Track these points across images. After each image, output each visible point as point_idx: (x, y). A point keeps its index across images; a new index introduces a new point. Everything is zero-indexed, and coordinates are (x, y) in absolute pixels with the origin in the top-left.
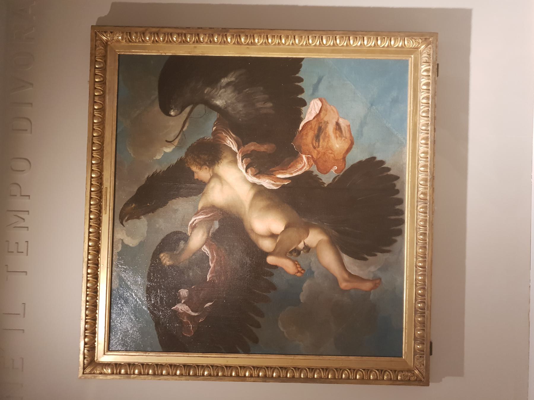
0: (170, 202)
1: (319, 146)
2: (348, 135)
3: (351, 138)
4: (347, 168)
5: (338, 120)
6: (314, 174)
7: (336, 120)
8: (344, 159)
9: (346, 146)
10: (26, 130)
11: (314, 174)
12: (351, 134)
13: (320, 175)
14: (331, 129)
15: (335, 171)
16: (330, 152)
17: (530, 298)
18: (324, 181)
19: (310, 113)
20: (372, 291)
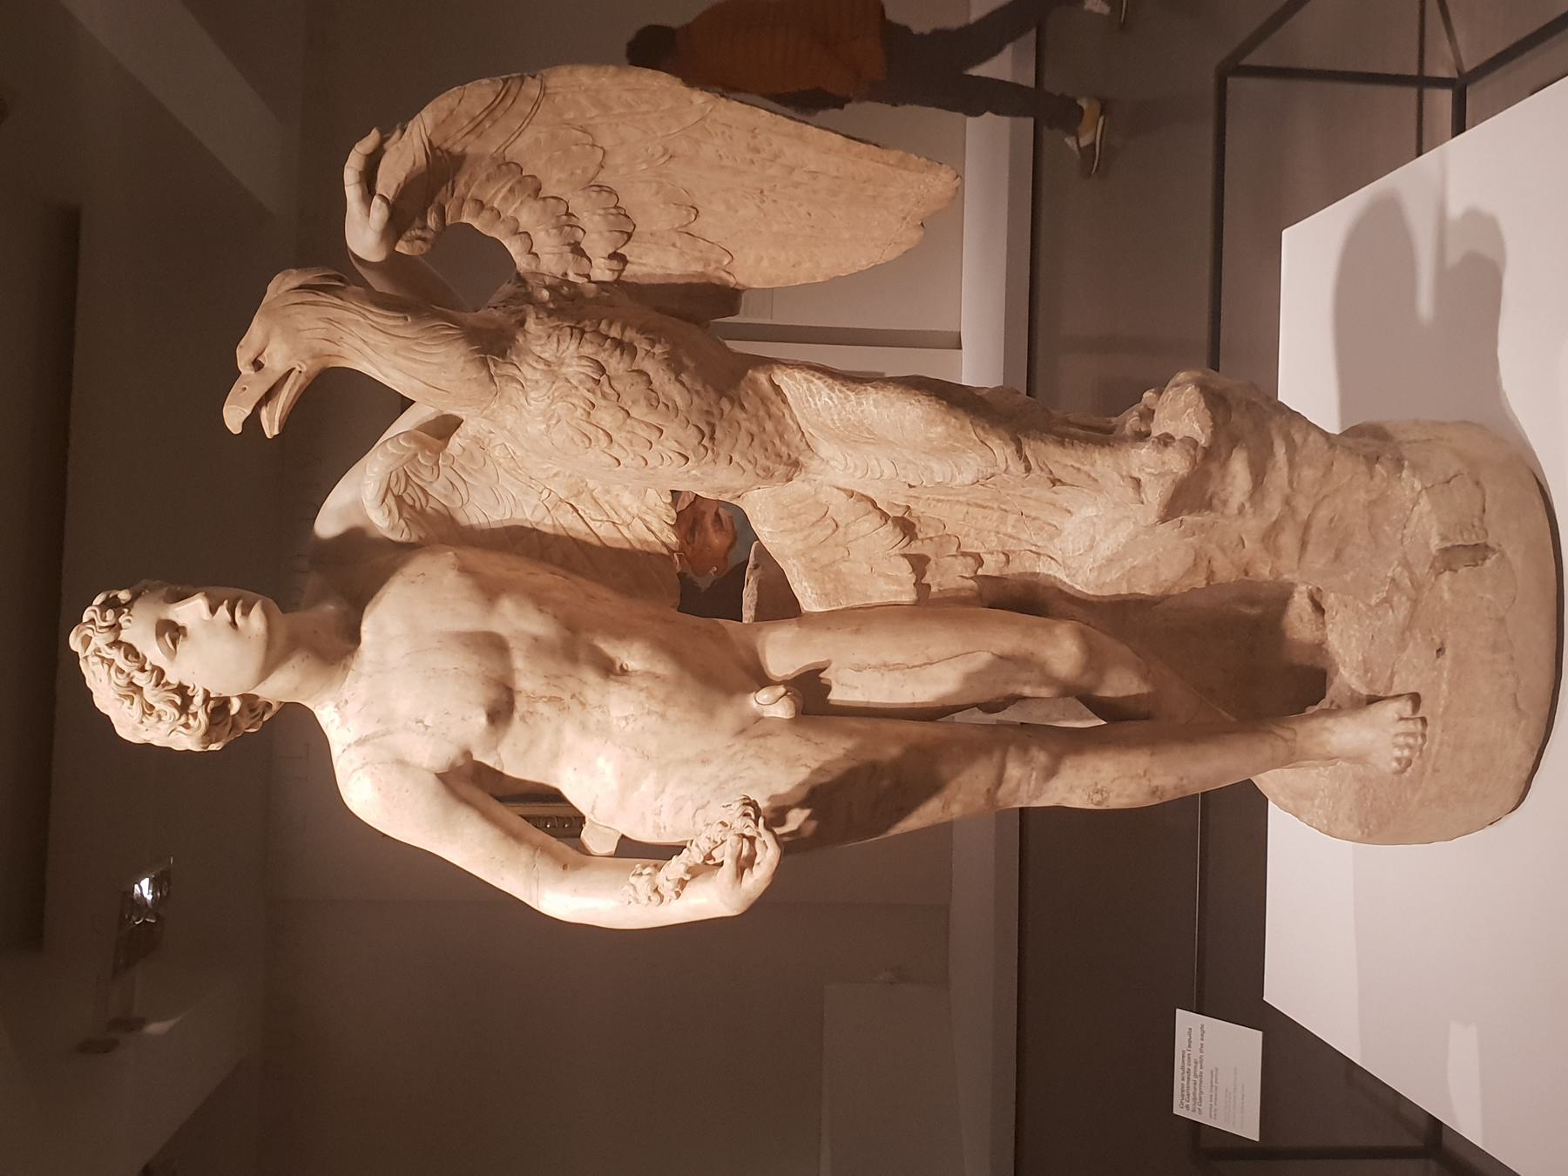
0: (679, 80)
1: (694, 541)
2: (730, 528)
3: (1050, 476)
4: (728, 569)
5: (718, 510)
6: (688, 576)
7: (714, 510)
8: (725, 558)
9: (728, 542)
10: (856, 688)
11: (688, 576)
12: (733, 526)
13: (696, 579)
14: (709, 520)
15: (715, 572)
16: (708, 549)
17: (446, 544)
18: (700, 585)
19: (683, 500)
20: (264, 413)
